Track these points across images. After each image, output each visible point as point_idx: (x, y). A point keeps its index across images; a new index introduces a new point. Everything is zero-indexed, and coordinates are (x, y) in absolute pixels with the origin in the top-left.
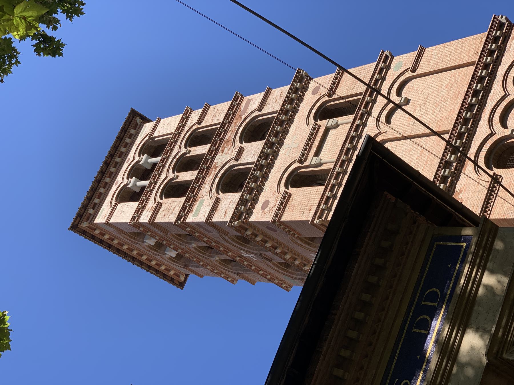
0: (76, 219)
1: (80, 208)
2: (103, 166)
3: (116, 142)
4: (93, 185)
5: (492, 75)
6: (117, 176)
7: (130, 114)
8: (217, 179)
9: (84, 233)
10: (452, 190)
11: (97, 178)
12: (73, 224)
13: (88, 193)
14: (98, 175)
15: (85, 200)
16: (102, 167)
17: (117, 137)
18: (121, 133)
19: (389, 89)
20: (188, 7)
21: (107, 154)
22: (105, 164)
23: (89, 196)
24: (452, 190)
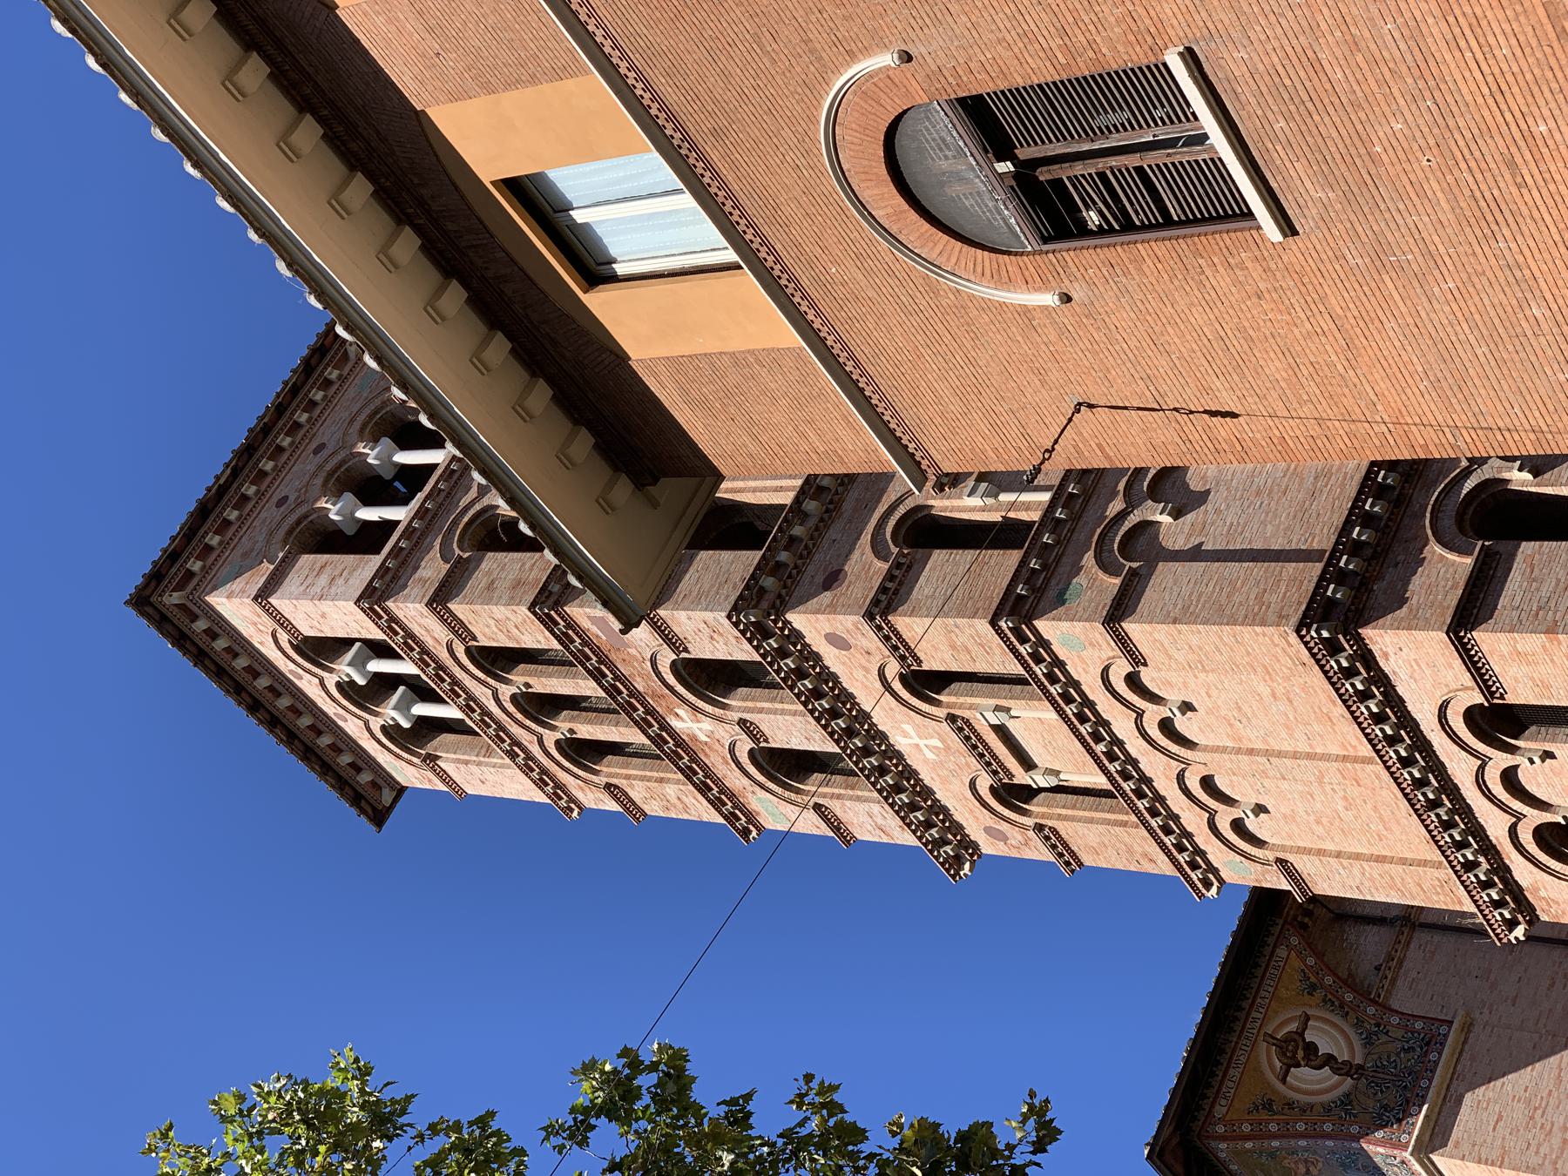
0: (362, 811)
1: (342, 796)
2: (259, 719)
3: (206, 670)
4: (347, 799)
5: (1465, 811)
6: (374, 760)
7: (143, 614)
8: (528, 723)
9: (161, 621)
10: (1514, 887)
11: (282, 740)
12: (371, 820)
13: (313, 769)
14: (277, 736)
15: (326, 781)
16: (261, 722)
17: (195, 665)
18: (186, 649)
19: (1180, 788)
20: (618, 201)
21: (231, 701)
22: (257, 711)
23: (321, 767)
24: (1514, 887)
